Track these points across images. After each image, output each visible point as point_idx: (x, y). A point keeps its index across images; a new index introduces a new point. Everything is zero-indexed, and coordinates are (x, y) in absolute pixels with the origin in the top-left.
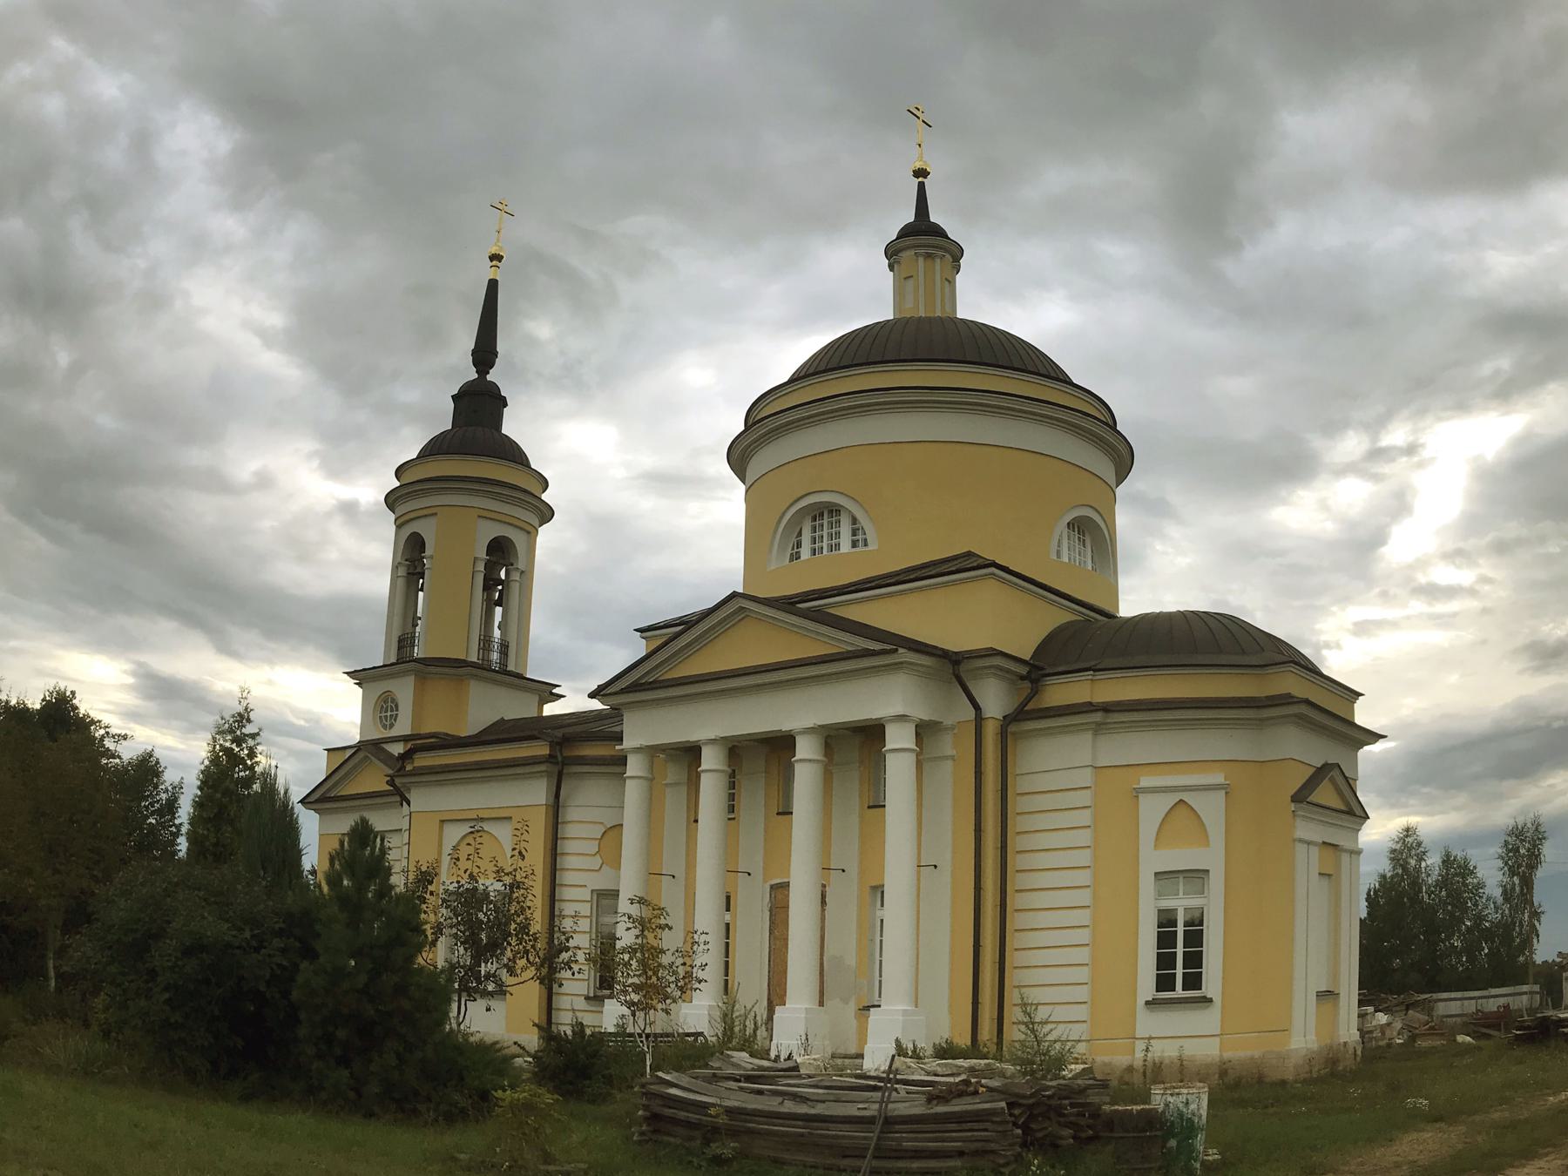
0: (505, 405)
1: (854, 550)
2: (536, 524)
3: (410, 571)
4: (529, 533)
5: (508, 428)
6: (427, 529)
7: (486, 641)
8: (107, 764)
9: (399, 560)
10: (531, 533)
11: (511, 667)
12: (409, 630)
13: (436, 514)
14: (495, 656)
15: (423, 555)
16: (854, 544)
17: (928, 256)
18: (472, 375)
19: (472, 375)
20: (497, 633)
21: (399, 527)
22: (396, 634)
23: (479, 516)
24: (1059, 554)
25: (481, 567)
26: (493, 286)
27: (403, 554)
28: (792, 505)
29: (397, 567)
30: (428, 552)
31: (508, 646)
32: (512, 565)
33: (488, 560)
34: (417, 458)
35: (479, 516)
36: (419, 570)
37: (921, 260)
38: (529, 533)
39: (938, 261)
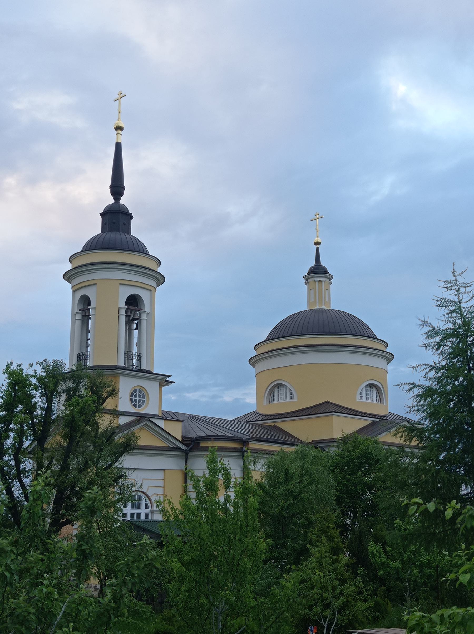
0: (132, 218)
1: (292, 400)
2: (155, 286)
3: (83, 315)
4: (150, 290)
5: (134, 232)
6: (90, 293)
7: (128, 355)
8: (434, 545)
9: (76, 310)
10: (151, 290)
11: (144, 367)
12: (84, 350)
13: (96, 284)
14: (134, 362)
15: (89, 307)
16: (291, 398)
17: (320, 281)
18: (111, 200)
19: (111, 200)
20: (135, 350)
21: (74, 291)
22: (76, 352)
23: (120, 284)
24: (361, 398)
25: (123, 312)
26: (118, 146)
27: (78, 306)
28: (270, 384)
29: (75, 314)
30: (92, 306)
31: (141, 356)
32: (142, 310)
33: (127, 308)
34: (83, 251)
35: (120, 284)
36: (87, 314)
37: (317, 283)
38: (150, 290)
39: (323, 282)
